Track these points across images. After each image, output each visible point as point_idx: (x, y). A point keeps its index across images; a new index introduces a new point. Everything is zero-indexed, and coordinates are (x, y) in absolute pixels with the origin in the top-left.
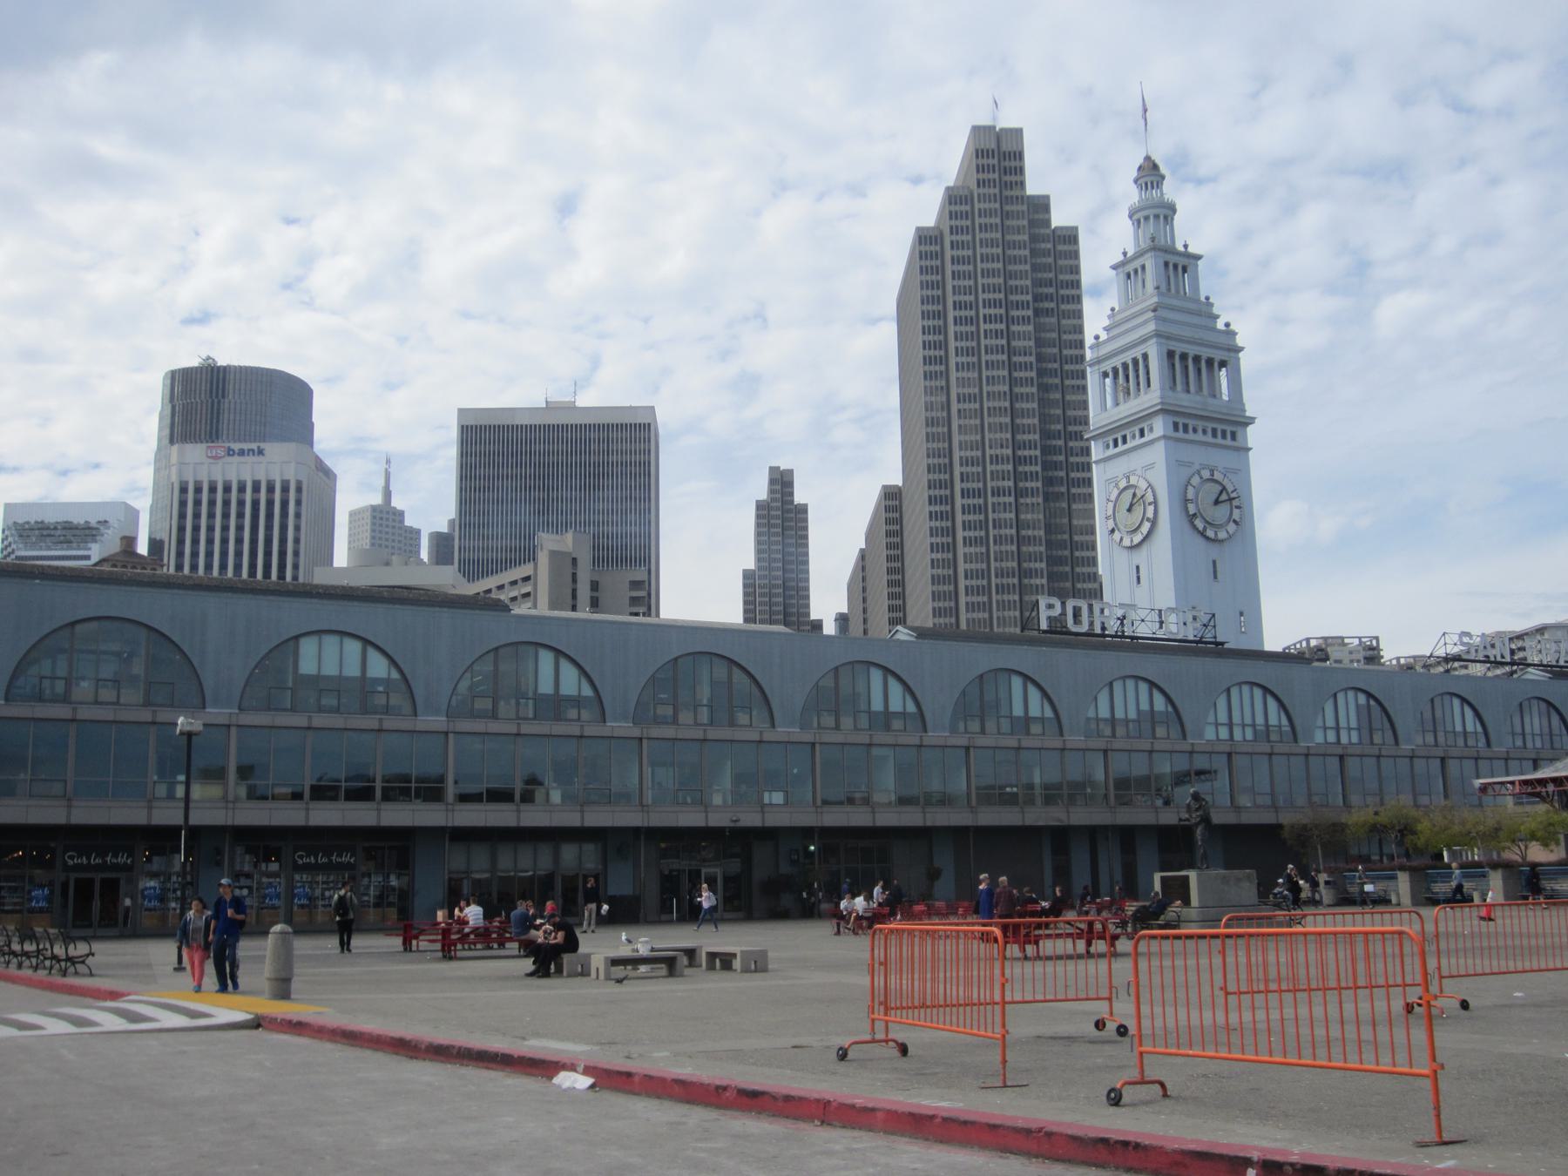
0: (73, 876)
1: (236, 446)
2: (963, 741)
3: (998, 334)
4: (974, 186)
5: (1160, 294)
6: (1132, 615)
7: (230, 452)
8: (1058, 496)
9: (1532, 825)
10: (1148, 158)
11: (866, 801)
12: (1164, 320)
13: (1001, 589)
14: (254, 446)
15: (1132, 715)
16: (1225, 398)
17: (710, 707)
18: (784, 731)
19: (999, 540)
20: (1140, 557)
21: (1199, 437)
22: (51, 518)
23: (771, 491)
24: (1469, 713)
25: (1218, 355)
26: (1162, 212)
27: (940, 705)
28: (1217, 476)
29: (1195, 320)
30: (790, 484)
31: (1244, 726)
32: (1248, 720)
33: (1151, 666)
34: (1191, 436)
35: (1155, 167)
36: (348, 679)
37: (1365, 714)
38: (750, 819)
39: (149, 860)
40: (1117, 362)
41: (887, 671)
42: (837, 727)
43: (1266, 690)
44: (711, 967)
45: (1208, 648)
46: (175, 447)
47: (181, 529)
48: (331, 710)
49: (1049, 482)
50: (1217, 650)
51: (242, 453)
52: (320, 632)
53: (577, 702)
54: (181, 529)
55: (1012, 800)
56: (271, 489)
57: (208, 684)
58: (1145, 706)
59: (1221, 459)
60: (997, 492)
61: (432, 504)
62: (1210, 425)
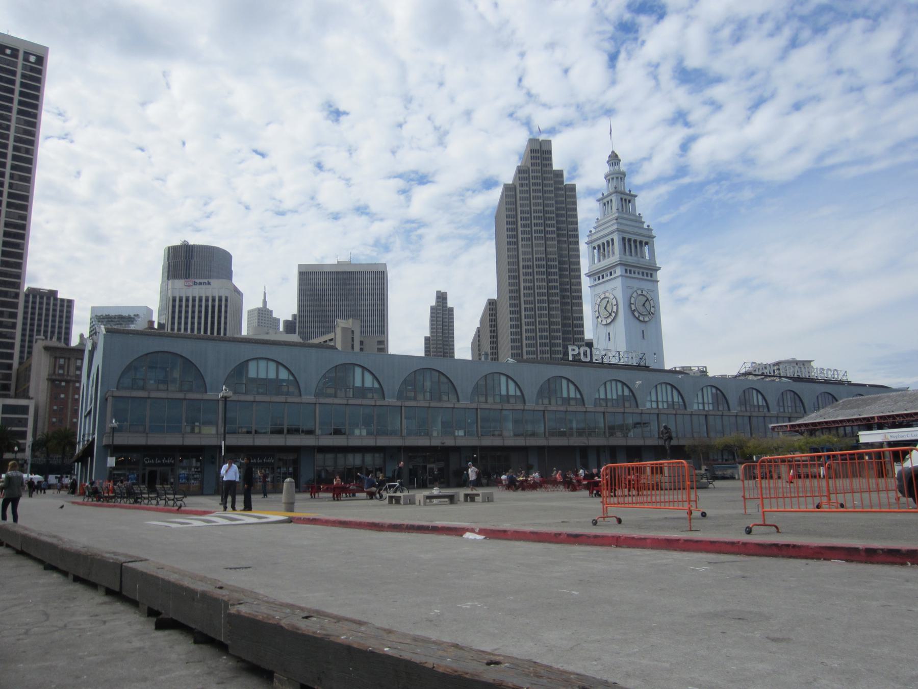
0: (148, 469)
1: (198, 281)
2: (542, 408)
3: (540, 232)
4: (529, 165)
5: (619, 212)
6: (609, 354)
7: (195, 283)
8: (567, 304)
9: (796, 444)
10: (613, 152)
11: (500, 435)
12: (621, 224)
13: (542, 345)
14: (206, 281)
15: (615, 397)
16: (647, 258)
17: (431, 392)
18: (463, 403)
19: (541, 323)
20: (610, 329)
21: (636, 275)
22: (112, 313)
23: (437, 302)
24: (760, 397)
25: (644, 240)
26: (619, 176)
27: (531, 392)
28: (644, 293)
29: (637, 224)
30: (446, 299)
31: (663, 402)
32: (665, 399)
33: (623, 375)
34: (633, 275)
35: (616, 156)
36: (271, 380)
37: (715, 398)
38: (449, 442)
39: (181, 461)
40: (600, 242)
41: (508, 377)
42: (486, 402)
43: (672, 386)
44: (466, 500)
45: (641, 368)
46: (170, 282)
47: (173, 318)
48: (262, 394)
49: (563, 297)
50: (647, 368)
51: (200, 284)
52: (257, 359)
53: (372, 390)
54: (173, 318)
55: (563, 434)
56: (214, 300)
57: (208, 380)
58: (620, 393)
59: (646, 286)
60: (540, 302)
61: (285, 306)
62: (641, 271)
